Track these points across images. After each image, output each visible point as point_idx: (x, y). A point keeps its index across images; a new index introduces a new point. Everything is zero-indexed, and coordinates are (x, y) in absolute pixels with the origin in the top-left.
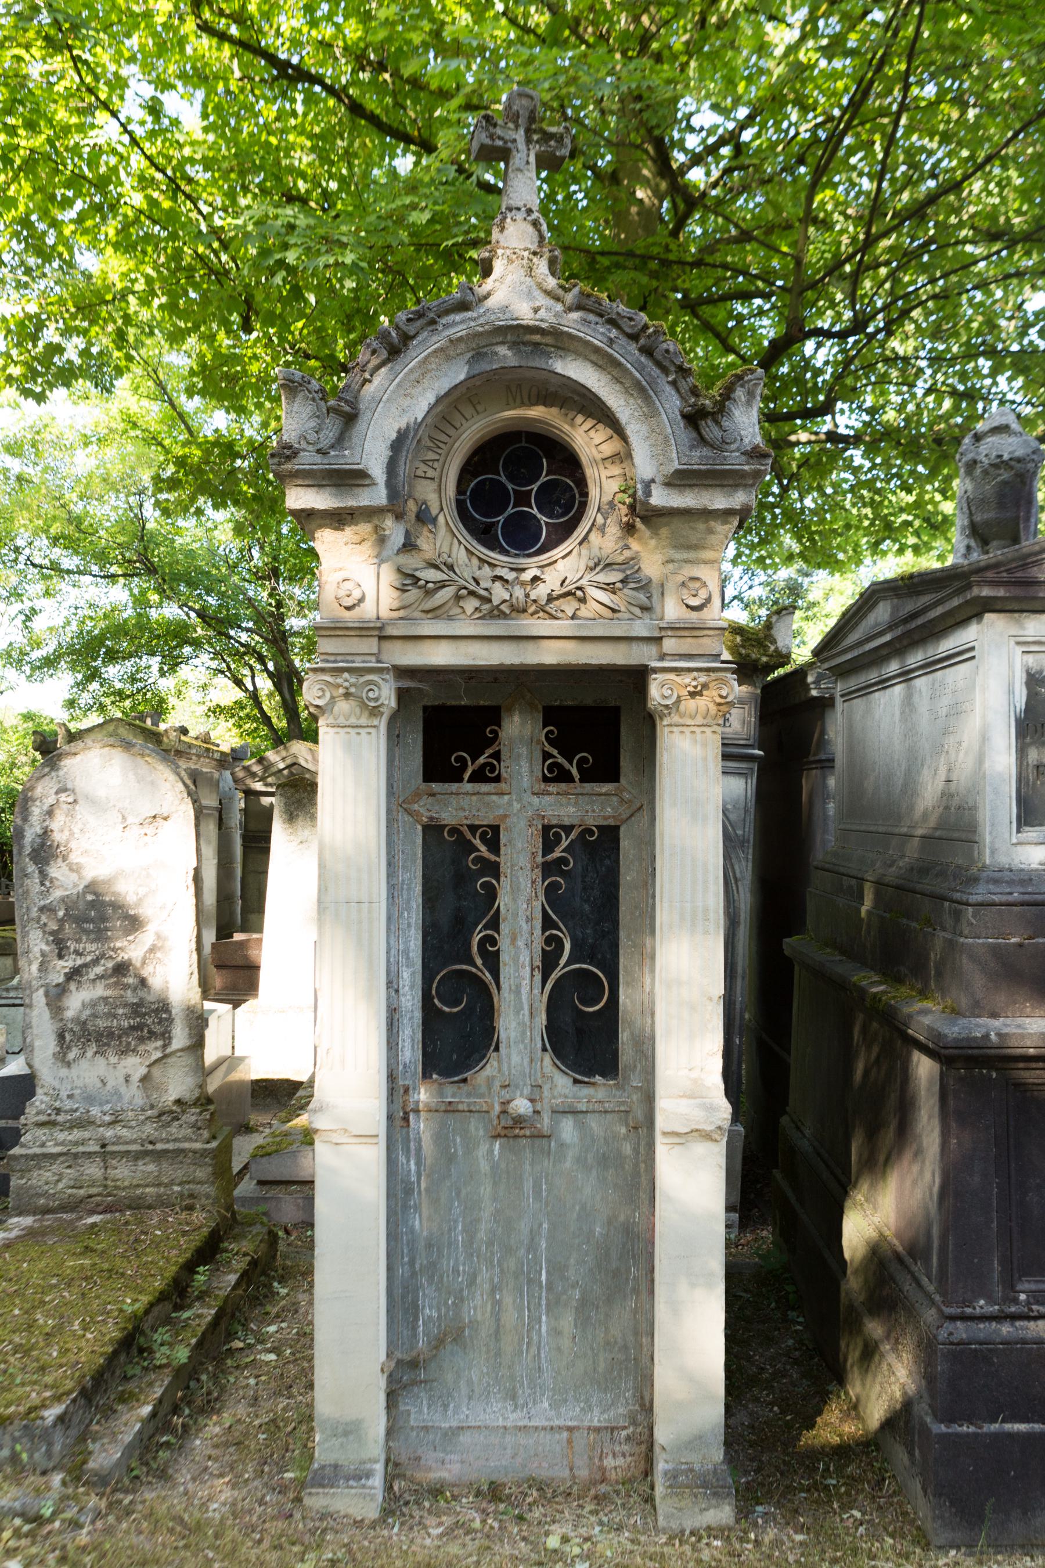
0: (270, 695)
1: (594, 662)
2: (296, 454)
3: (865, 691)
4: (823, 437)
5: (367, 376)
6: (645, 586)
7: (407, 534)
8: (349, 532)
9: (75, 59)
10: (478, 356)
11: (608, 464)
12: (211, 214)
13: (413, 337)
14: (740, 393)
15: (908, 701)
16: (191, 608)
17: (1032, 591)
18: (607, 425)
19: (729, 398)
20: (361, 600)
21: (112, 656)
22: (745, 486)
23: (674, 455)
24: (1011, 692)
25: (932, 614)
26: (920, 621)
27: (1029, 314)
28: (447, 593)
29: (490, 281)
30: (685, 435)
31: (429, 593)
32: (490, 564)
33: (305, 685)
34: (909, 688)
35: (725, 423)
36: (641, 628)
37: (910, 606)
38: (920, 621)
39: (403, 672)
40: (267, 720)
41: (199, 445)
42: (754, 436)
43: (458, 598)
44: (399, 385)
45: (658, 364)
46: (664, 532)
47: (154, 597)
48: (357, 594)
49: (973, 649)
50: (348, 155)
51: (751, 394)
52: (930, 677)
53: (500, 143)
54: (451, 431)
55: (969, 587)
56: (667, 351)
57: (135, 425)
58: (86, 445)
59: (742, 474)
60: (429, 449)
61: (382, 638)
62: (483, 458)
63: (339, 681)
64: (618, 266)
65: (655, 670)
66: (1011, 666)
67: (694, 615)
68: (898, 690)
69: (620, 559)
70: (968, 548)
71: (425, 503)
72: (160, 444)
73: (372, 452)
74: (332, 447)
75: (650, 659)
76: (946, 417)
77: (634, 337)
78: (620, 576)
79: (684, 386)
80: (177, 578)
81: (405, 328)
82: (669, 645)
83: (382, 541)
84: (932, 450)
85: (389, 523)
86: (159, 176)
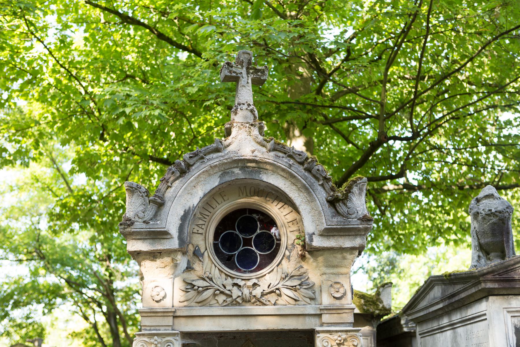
0: (104, 325)
1: (286, 328)
2: (132, 224)
3: (431, 332)
4: (401, 187)
5: (169, 184)
6: (311, 287)
7: (189, 262)
8: (159, 262)
9: (26, 20)
10: (224, 173)
11: (290, 224)
12: (87, 86)
13: (193, 165)
14: (355, 189)
15: (455, 339)
16: (61, 278)
17: (513, 284)
18: (289, 205)
19: (350, 192)
20: (164, 297)
21: (16, 305)
22: (361, 235)
23: (324, 221)
24: (507, 338)
25: (463, 295)
26: (457, 298)
27: (502, 123)
28: (209, 292)
29: (230, 138)
30: (329, 210)
31: (199, 293)
32: (231, 277)
33: (134, 343)
34: (455, 333)
35: (349, 204)
36: (310, 309)
37: (451, 290)
38: (457, 298)
39: (186, 335)
40: (101, 340)
41: (74, 197)
42: (363, 210)
43: (215, 295)
44: (185, 189)
45: (314, 176)
46: (321, 259)
47: (42, 271)
48: (162, 294)
49: (485, 315)
50: (155, 54)
51: (361, 190)
52: (464, 327)
53: (235, 74)
54: (211, 210)
55: (479, 283)
56: (318, 170)
57: (38, 181)
58: (12, 190)
59: (359, 230)
60: (200, 219)
61: (175, 317)
62: (227, 222)
63: (152, 341)
64: (291, 108)
65: (319, 332)
66: (506, 324)
67: (337, 302)
68: (449, 333)
69: (298, 273)
70: (479, 257)
71: (197, 246)
72: (51, 190)
73: (171, 221)
74: (151, 219)
75: (316, 325)
76: (464, 175)
77: (302, 164)
78: (299, 282)
79: (327, 187)
80: (55, 262)
81: (188, 161)
82: (326, 318)
83: (176, 266)
84: (458, 194)
85: (179, 257)
86: (62, 70)
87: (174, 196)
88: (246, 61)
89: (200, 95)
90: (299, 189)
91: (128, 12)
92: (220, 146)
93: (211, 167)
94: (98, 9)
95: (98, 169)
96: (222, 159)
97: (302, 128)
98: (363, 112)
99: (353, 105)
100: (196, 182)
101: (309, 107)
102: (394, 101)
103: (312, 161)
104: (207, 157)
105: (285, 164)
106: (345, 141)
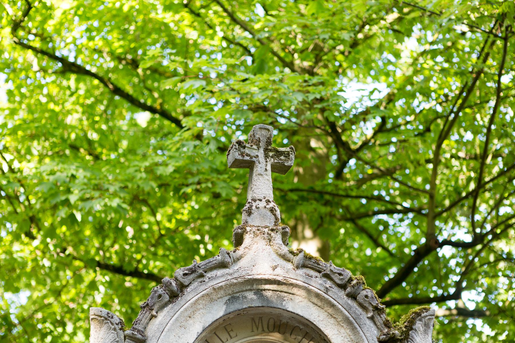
5: (154, 313)
10: (233, 299)
13: (188, 286)
14: (419, 325)
19: (412, 329)
44: (177, 320)
56: (366, 296)
64: (303, 199)
77: (343, 287)
87: (161, 330)
88: (263, 140)
89: (175, 178)
90: (339, 324)
91: (68, 57)
92: (228, 259)
93: (214, 289)
94: (30, 52)
95: (19, 277)
96: (229, 277)
97: (315, 227)
98: (397, 204)
99: (383, 193)
100: (191, 310)
101: (327, 197)
102: (447, 190)
103: (357, 283)
104: (209, 275)
105: (319, 287)
106: (372, 244)
